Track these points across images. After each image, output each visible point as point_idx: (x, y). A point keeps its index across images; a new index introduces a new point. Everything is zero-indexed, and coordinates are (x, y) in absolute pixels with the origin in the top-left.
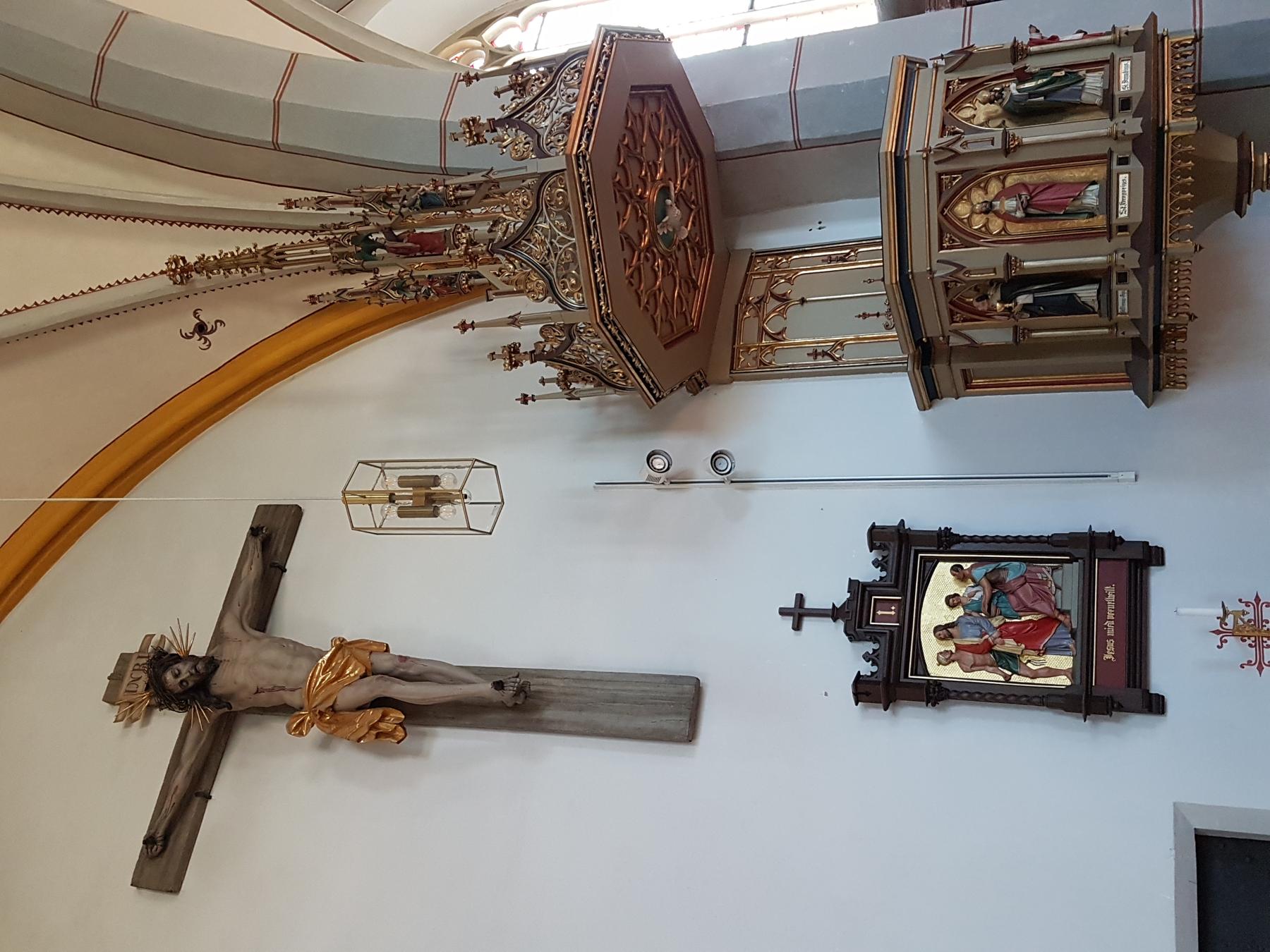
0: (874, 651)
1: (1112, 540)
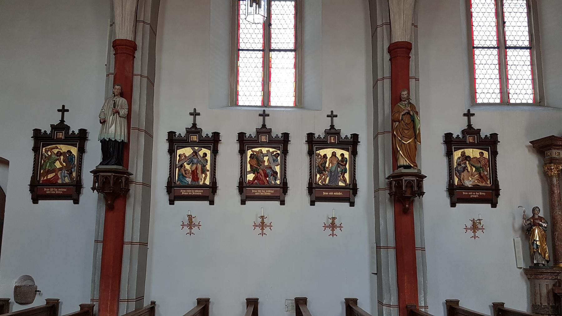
0: (279, 137)
1: (498, 195)
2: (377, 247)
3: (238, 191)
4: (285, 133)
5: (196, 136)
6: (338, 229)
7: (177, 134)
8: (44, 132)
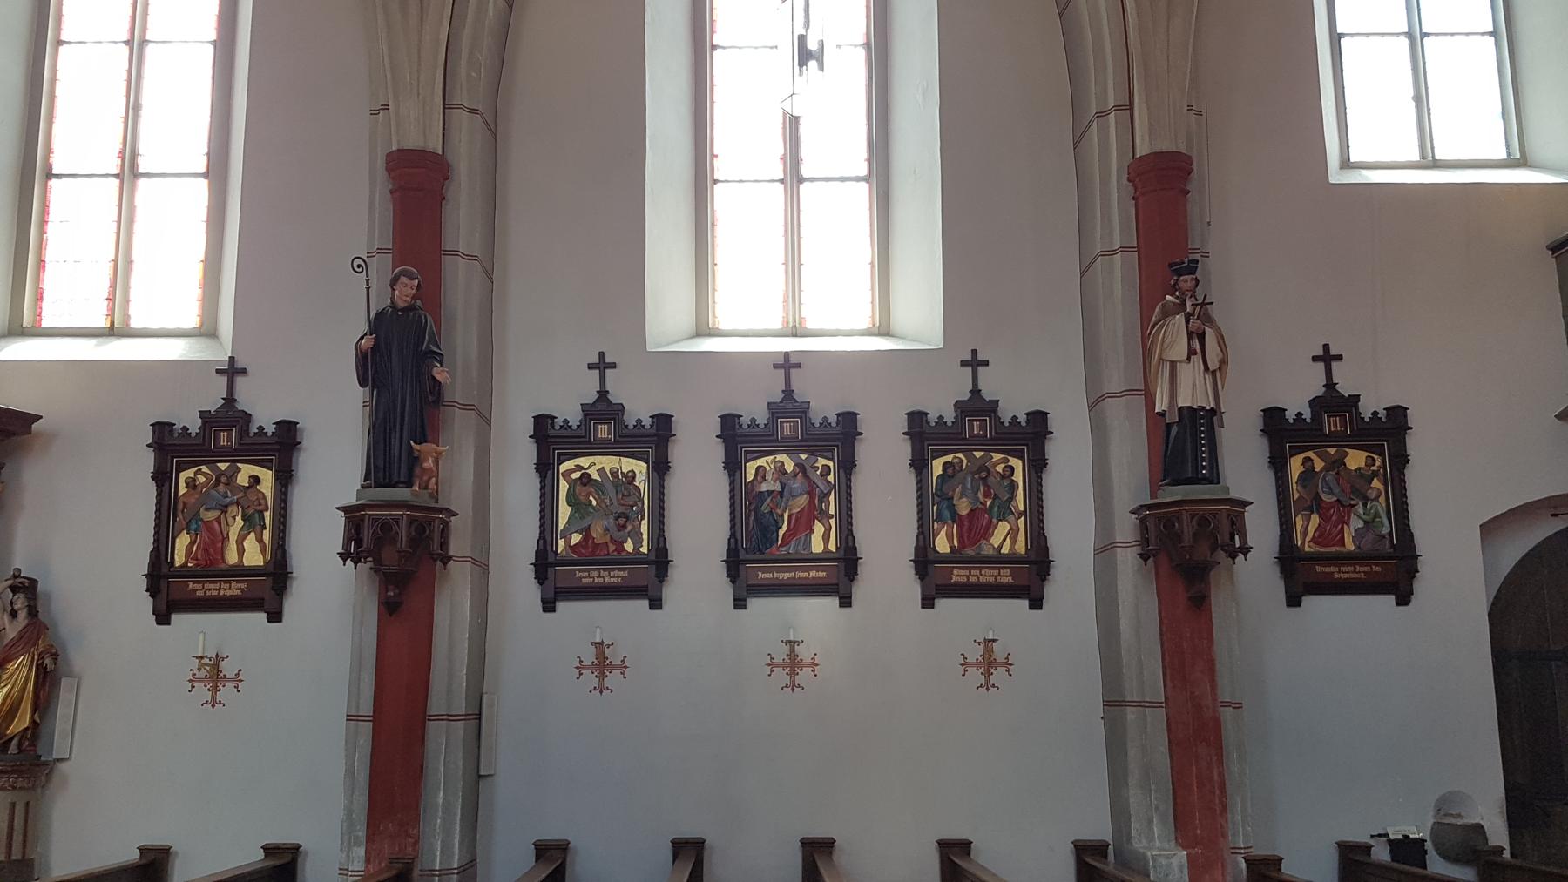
0: (758, 425)
1: (1412, 572)
2: (478, 717)
3: (726, 575)
4: (729, 415)
5: (606, 426)
6: (1001, 670)
7: (559, 421)
8: (180, 431)
